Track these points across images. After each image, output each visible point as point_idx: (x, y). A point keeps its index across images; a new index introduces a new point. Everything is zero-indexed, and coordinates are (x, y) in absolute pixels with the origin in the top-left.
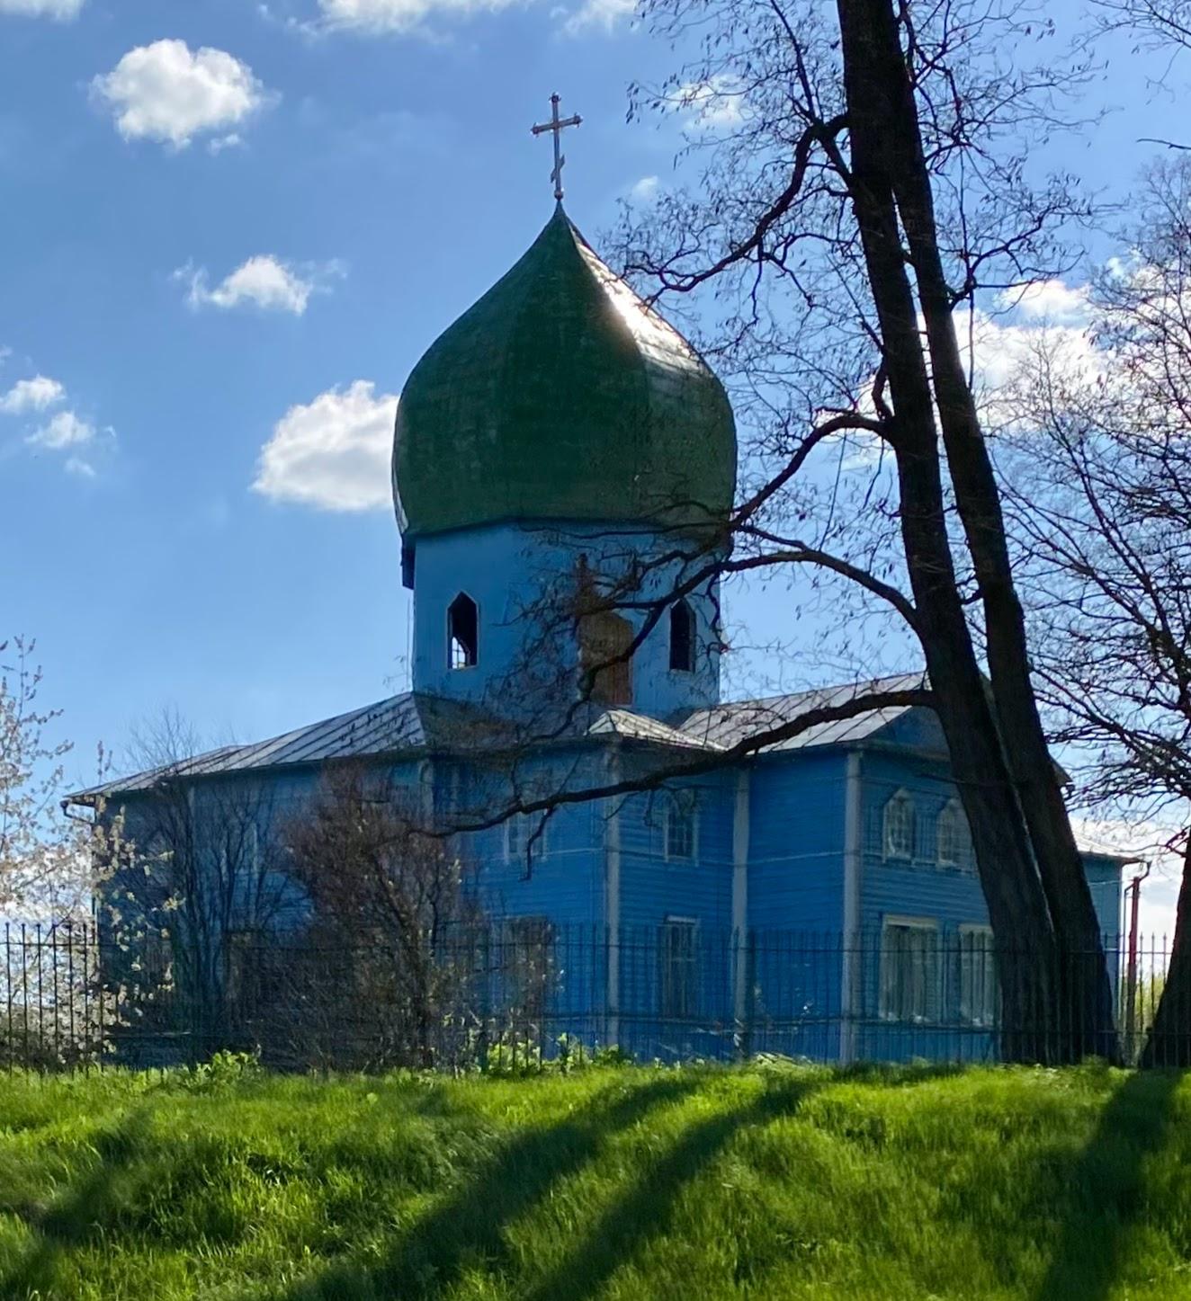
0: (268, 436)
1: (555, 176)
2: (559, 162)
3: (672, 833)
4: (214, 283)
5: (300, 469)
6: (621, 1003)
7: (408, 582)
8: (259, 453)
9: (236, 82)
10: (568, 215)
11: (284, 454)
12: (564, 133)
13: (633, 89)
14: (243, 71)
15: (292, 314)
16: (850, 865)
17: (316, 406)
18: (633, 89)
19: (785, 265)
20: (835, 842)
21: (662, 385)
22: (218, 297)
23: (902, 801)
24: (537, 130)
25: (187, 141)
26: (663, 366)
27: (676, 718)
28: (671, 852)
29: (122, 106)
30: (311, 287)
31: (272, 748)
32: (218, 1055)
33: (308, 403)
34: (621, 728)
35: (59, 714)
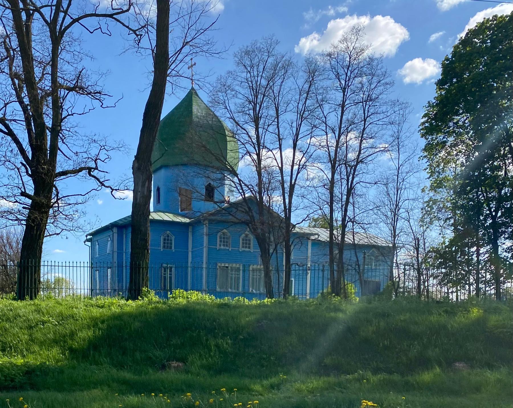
6: (208, 287)
28: (164, 247)
29: (405, 76)
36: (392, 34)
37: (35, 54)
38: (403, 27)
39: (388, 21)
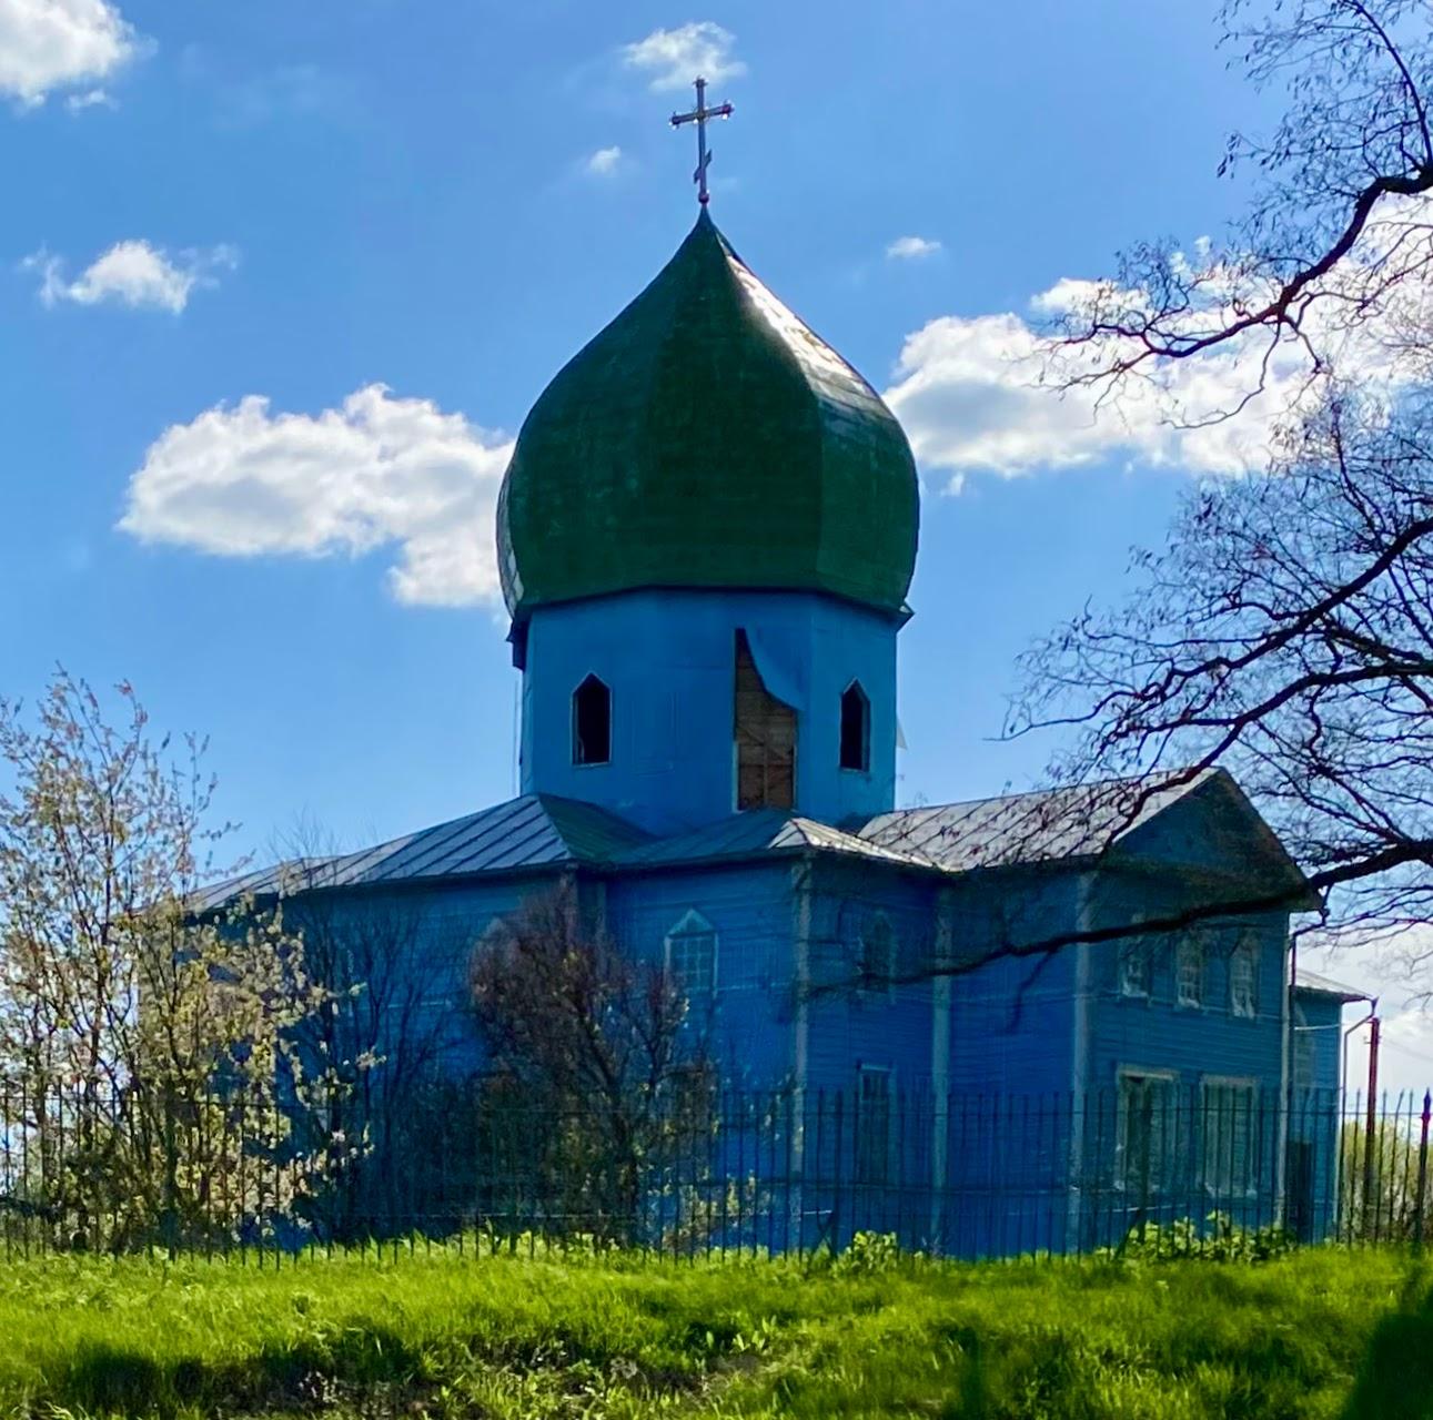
0: (139, 463)
1: (700, 175)
2: (705, 159)
4: (72, 275)
5: (181, 502)
7: (520, 661)
8: (127, 484)
9: (101, 27)
10: (714, 222)
11: (159, 484)
12: (714, 125)
13: (1234, 140)
14: (110, 14)
15: (166, 314)
16: (1080, 1004)
17: (197, 427)
18: (1234, 140)
19: (1301, 328)
21: (839, 428)
22: (77, 292)
24: (677, 121)
25: (39, 99)
26: (838, 406)
27: (851, 825)
30: (191, 280)
31: (374, 861)
32: (528, 1234)
33: (188, 422)
34: (815, 841)
35: (236, 828)
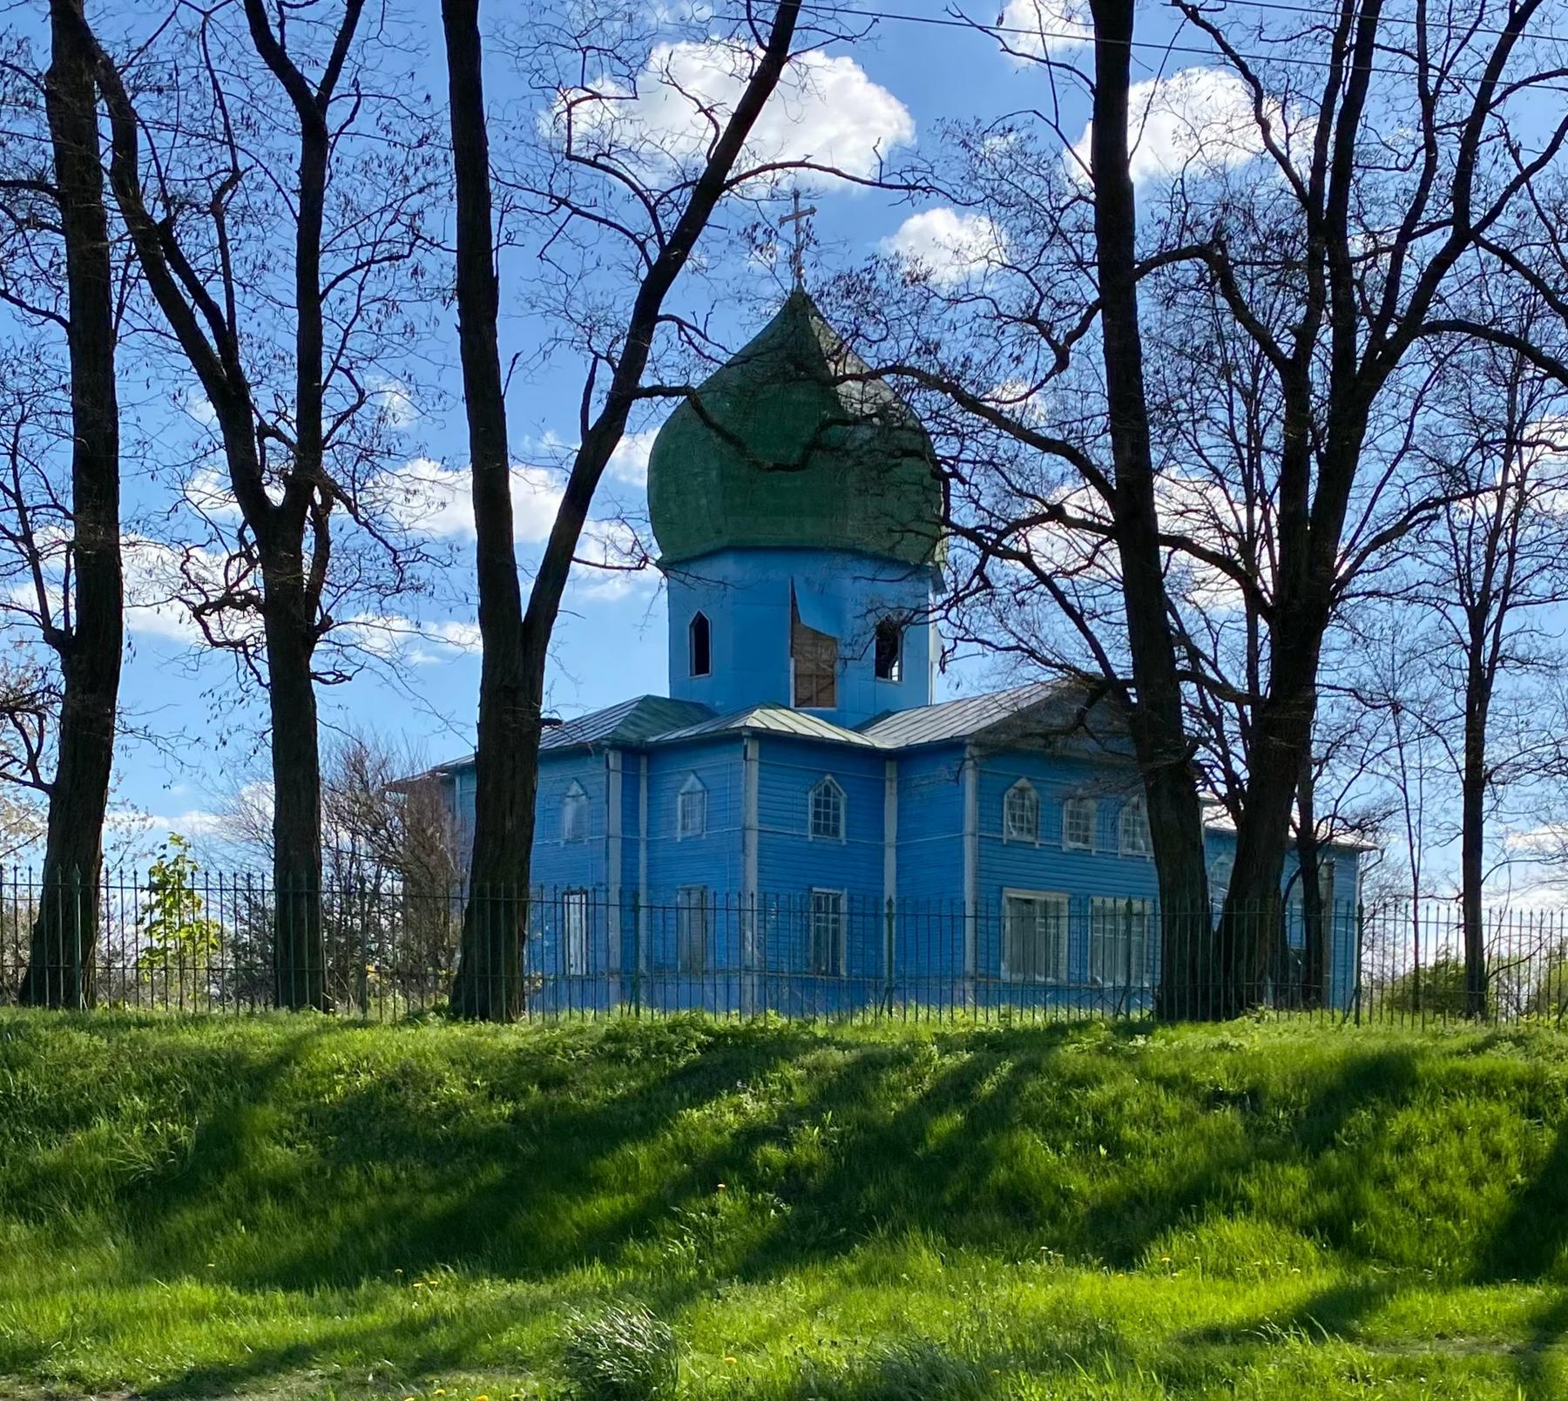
3: (817, 815)
16: (969, 845)
20: (958, 826)
23: (1022, 790)
28: (816, 829)
36: (863, 119)
37: (1472, 102)
38: (893, 100)
39: (844, 73)
